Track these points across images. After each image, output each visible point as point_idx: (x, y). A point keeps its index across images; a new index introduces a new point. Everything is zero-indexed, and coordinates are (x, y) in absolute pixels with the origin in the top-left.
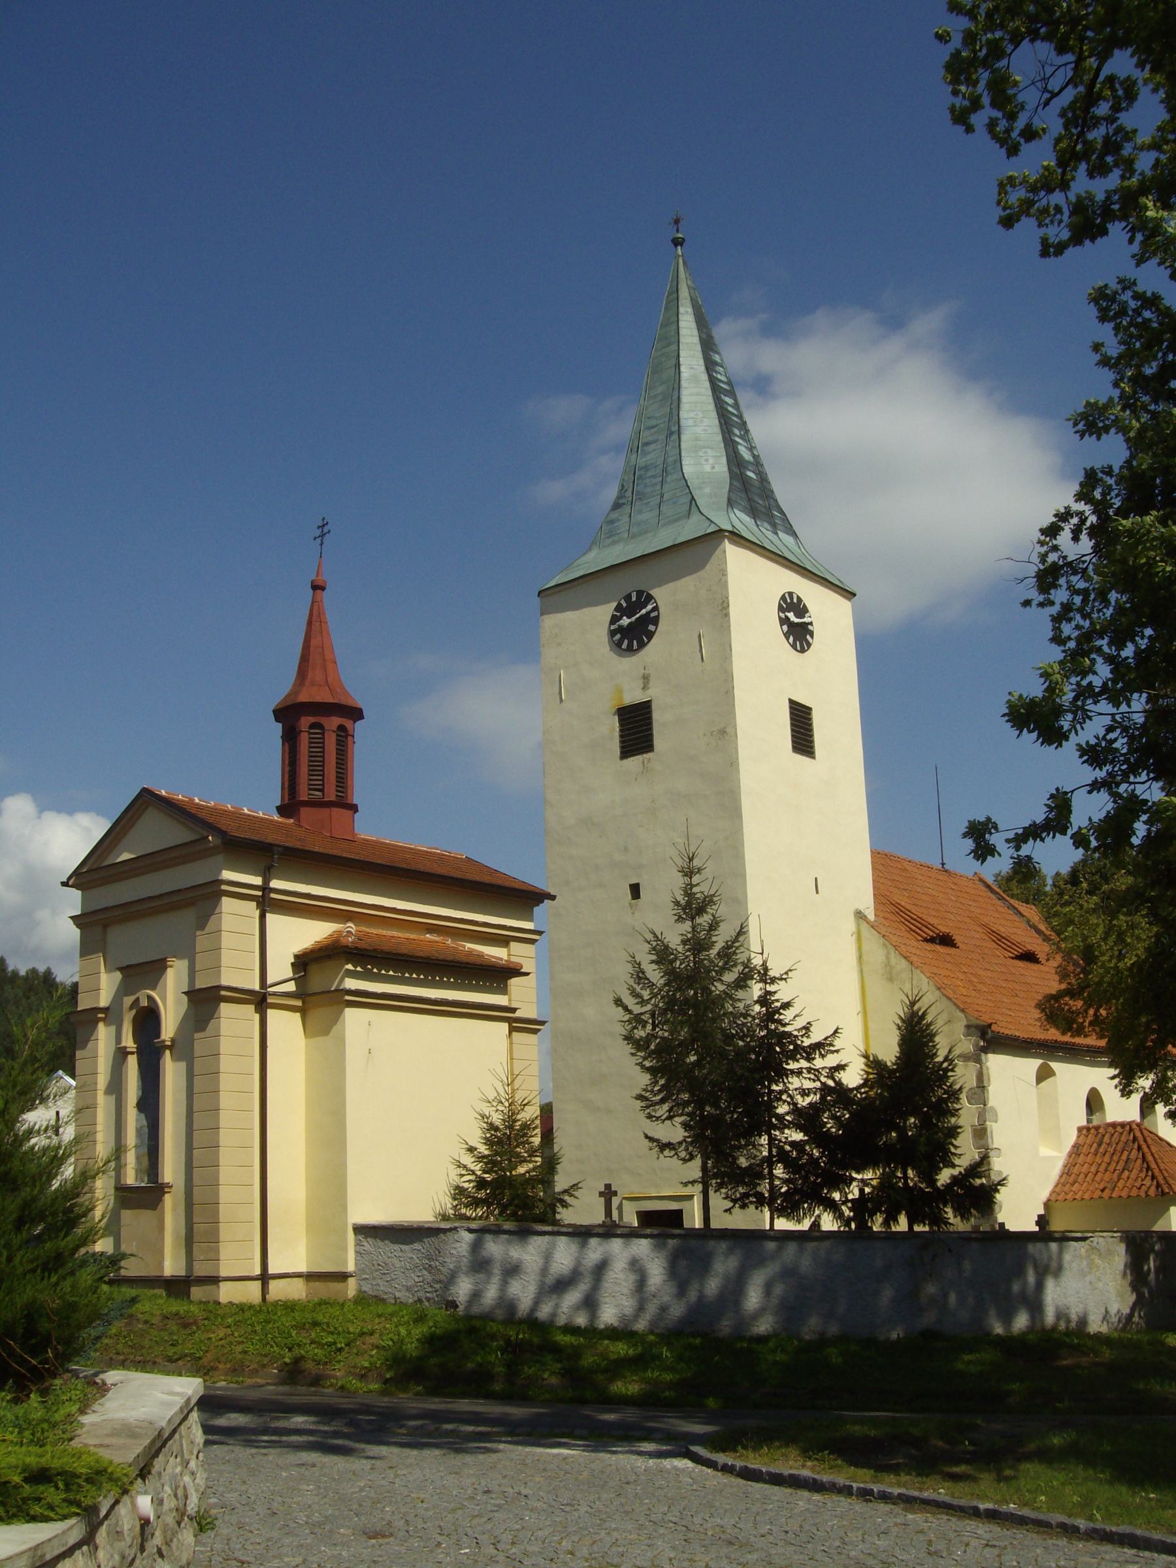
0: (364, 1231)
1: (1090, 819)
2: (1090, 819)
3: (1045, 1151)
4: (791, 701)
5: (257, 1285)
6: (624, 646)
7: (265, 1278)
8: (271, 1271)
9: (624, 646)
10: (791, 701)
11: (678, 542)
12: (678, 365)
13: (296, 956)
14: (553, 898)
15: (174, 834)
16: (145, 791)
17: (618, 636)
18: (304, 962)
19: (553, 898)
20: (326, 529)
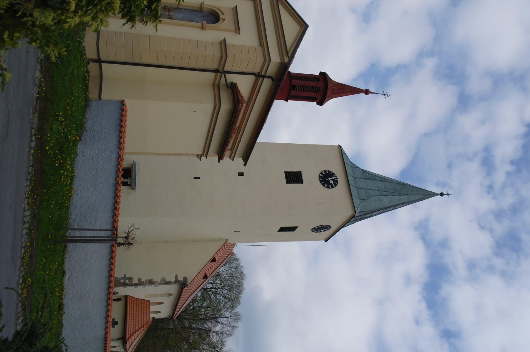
0: (122, 103)
1: (176, 277)
2: (176, 277)
3: (143, 295)
4: (297, 227)
5: (95, 57)
6: (321, 175)
7: (99, 61)
8: (103, 64)
9: (321, 175)
10: (297, 227)
11: (348, 175)
12: (405, 195)
13: (236, 84)
14: (245, 165)
15: (290, 39)
16: (306, 26)
17: (324, 173)
18: (233, 87)
19: (245, 165)
20: (386, 96)
